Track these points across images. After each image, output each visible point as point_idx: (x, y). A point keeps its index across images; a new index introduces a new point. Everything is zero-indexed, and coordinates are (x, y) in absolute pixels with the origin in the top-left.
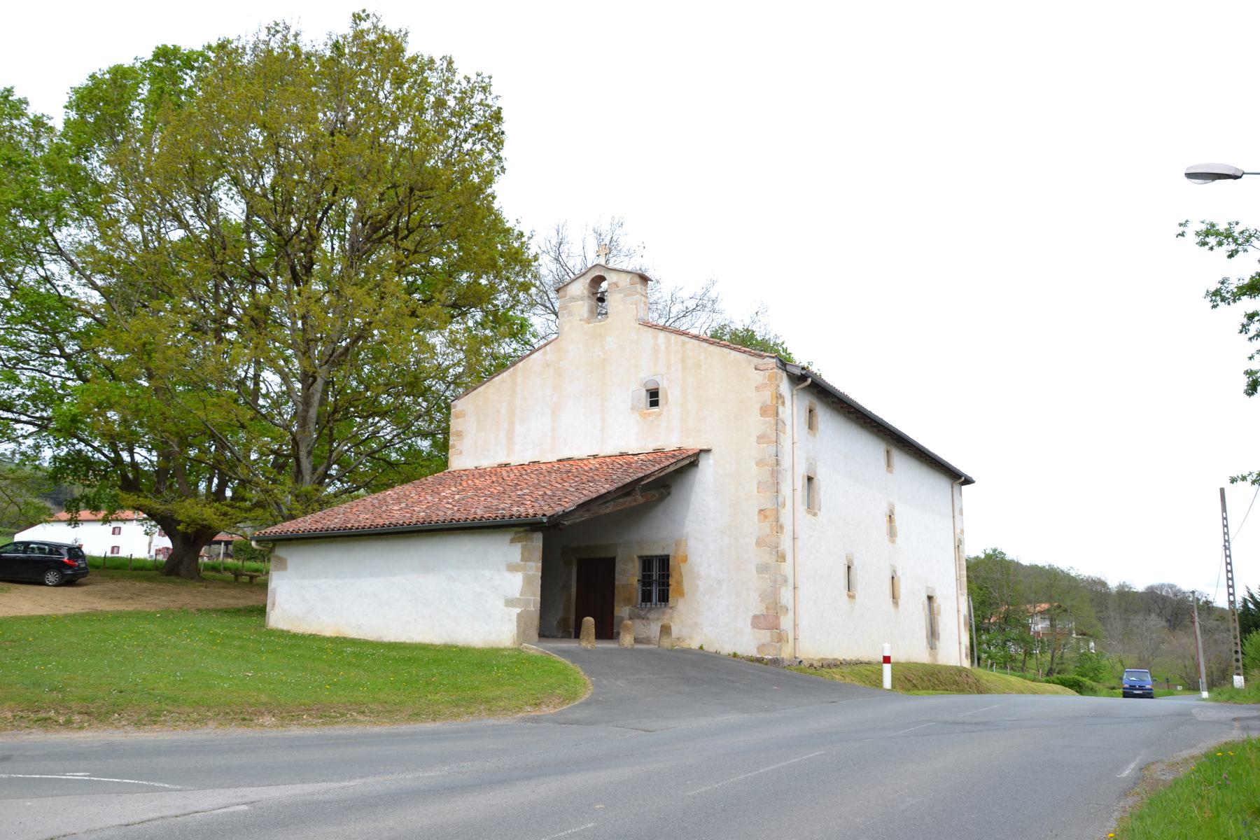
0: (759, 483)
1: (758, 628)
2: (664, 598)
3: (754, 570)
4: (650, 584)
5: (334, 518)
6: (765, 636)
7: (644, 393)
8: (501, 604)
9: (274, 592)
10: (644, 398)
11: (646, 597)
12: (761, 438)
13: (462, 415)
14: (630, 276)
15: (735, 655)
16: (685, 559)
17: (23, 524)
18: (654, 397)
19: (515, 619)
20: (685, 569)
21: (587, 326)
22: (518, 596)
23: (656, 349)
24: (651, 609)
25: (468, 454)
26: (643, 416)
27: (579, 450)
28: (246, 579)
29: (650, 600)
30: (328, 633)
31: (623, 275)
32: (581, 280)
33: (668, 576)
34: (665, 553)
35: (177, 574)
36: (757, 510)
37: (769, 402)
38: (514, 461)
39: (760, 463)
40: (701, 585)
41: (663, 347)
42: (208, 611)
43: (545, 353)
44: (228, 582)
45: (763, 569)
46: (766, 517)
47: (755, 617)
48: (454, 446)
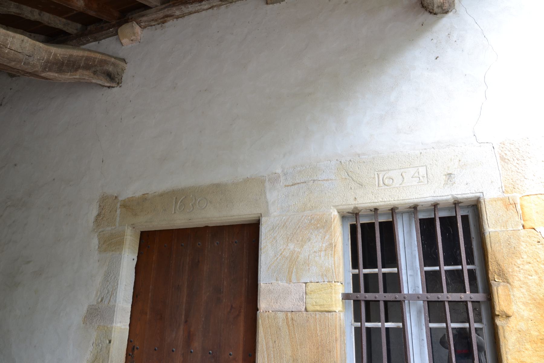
4: (395, 310)
34: (463, 191)
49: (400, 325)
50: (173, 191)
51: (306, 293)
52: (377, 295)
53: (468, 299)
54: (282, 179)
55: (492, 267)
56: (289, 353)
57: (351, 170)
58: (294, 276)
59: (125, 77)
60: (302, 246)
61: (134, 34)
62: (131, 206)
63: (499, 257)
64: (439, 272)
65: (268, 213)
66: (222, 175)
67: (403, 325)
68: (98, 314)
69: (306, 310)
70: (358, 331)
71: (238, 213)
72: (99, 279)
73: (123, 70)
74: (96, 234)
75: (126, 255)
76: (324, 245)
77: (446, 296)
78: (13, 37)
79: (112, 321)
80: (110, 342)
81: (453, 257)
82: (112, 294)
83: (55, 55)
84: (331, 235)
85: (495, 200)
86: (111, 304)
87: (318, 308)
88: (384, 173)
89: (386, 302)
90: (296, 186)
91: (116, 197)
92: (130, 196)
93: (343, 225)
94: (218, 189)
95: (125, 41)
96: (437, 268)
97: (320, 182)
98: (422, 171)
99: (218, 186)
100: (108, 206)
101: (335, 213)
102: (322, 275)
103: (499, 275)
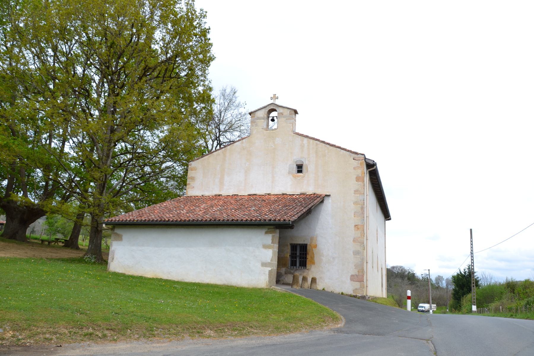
0: (355, 213)
1: (354, 281)
2: (303, 264)
3: (352, 253)
4: (296, 258)
5: (134, 216)
6: (357, 285)
7: (295, 166)
8: (259, 265)
9: (113, 252)
10: (295, 169)
11: (293, 264)
12: (356, 191)
13: (195, 169)
14: (289, 110)
15: (342, 294)
16: (316, 246)
17: (229, 198)
18: (300, 169)
19: (267, 273)
20: (315, 251)
21: (265, 132)
22: (269, 261)
23: (302, 146)
24: (297, 270)
25: (194, 190)
26: (294, 177)
27: (260, 190)
28: (47, 243)
29: (296, 265)
30: (149, 275)
31: (286, 110)
32: (263, 110)
33: (306, 254)
34: (305, 243)
35: (15, 239)
36: (353, 225)
37: (360, 175)
38: (224, 193)
39: (355, 203)
40: (324, 259)
41: (306, 145)
42: (51, 259)
43: (242, 143)
44: (39, 244)
45: (356, 253)
46: (358, 229)
47: (352, 276)
48: (189, 184)
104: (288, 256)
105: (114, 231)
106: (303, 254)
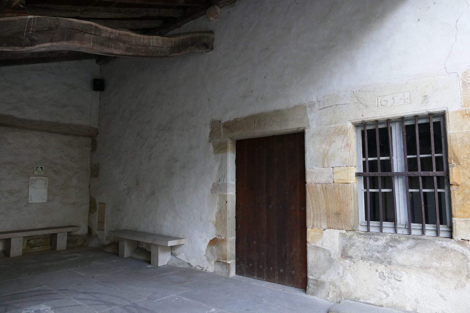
4: (388, 182)
29: (390, 217)
34: (434, 107)
49: (391, 190)
50: (252, 116)
51: (333, 173)
52: (376, 173)
53: (434, 175)
54: (317, 105)
55: (450, 155)
56: (325, 206)
57: (360, 97)
58: (326, 164)
59: (215, 44)
60: (330, 146)
61: (216, 13)
62: (230, 126)
63: (455, 149)
64: (431, 158)
65: (309, 126)
66: (280, 104)
67: (393, 190)
68: (218, 187)
69: (333, 182)
70: (365, 193)
71: (292, 126)
72: (216, 169)
73: (213, 39)
74: (211, 144)
75: (229, 155)
76: (343, 145)
77: (420, 173)
78: (153, 39)
79: (227, 192)
80: (226, 202)
81: (426, 149)
82: (225, 177)
83: (175, 42)
84: (348, 138)
85: (456, 112)
86: (225, 182)
87: (340, 181)
88: (381, 97)
89: (438, 178)
90: (326, 109)
91: (220, 121)
92: (228, 120)
93: (356, 131)
94: (278, 113)
95: (212, 19)
96: (415, 156)
97: (340, 106)
98: (407, 95)
99: (278, 111)
100: (216, 126)
101: (350, 125)
102: (343, 163)
103: (454, 160)
104: (353, 179)
105: (425, 234)
106: (427, 165)
